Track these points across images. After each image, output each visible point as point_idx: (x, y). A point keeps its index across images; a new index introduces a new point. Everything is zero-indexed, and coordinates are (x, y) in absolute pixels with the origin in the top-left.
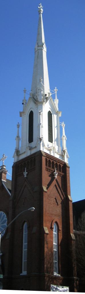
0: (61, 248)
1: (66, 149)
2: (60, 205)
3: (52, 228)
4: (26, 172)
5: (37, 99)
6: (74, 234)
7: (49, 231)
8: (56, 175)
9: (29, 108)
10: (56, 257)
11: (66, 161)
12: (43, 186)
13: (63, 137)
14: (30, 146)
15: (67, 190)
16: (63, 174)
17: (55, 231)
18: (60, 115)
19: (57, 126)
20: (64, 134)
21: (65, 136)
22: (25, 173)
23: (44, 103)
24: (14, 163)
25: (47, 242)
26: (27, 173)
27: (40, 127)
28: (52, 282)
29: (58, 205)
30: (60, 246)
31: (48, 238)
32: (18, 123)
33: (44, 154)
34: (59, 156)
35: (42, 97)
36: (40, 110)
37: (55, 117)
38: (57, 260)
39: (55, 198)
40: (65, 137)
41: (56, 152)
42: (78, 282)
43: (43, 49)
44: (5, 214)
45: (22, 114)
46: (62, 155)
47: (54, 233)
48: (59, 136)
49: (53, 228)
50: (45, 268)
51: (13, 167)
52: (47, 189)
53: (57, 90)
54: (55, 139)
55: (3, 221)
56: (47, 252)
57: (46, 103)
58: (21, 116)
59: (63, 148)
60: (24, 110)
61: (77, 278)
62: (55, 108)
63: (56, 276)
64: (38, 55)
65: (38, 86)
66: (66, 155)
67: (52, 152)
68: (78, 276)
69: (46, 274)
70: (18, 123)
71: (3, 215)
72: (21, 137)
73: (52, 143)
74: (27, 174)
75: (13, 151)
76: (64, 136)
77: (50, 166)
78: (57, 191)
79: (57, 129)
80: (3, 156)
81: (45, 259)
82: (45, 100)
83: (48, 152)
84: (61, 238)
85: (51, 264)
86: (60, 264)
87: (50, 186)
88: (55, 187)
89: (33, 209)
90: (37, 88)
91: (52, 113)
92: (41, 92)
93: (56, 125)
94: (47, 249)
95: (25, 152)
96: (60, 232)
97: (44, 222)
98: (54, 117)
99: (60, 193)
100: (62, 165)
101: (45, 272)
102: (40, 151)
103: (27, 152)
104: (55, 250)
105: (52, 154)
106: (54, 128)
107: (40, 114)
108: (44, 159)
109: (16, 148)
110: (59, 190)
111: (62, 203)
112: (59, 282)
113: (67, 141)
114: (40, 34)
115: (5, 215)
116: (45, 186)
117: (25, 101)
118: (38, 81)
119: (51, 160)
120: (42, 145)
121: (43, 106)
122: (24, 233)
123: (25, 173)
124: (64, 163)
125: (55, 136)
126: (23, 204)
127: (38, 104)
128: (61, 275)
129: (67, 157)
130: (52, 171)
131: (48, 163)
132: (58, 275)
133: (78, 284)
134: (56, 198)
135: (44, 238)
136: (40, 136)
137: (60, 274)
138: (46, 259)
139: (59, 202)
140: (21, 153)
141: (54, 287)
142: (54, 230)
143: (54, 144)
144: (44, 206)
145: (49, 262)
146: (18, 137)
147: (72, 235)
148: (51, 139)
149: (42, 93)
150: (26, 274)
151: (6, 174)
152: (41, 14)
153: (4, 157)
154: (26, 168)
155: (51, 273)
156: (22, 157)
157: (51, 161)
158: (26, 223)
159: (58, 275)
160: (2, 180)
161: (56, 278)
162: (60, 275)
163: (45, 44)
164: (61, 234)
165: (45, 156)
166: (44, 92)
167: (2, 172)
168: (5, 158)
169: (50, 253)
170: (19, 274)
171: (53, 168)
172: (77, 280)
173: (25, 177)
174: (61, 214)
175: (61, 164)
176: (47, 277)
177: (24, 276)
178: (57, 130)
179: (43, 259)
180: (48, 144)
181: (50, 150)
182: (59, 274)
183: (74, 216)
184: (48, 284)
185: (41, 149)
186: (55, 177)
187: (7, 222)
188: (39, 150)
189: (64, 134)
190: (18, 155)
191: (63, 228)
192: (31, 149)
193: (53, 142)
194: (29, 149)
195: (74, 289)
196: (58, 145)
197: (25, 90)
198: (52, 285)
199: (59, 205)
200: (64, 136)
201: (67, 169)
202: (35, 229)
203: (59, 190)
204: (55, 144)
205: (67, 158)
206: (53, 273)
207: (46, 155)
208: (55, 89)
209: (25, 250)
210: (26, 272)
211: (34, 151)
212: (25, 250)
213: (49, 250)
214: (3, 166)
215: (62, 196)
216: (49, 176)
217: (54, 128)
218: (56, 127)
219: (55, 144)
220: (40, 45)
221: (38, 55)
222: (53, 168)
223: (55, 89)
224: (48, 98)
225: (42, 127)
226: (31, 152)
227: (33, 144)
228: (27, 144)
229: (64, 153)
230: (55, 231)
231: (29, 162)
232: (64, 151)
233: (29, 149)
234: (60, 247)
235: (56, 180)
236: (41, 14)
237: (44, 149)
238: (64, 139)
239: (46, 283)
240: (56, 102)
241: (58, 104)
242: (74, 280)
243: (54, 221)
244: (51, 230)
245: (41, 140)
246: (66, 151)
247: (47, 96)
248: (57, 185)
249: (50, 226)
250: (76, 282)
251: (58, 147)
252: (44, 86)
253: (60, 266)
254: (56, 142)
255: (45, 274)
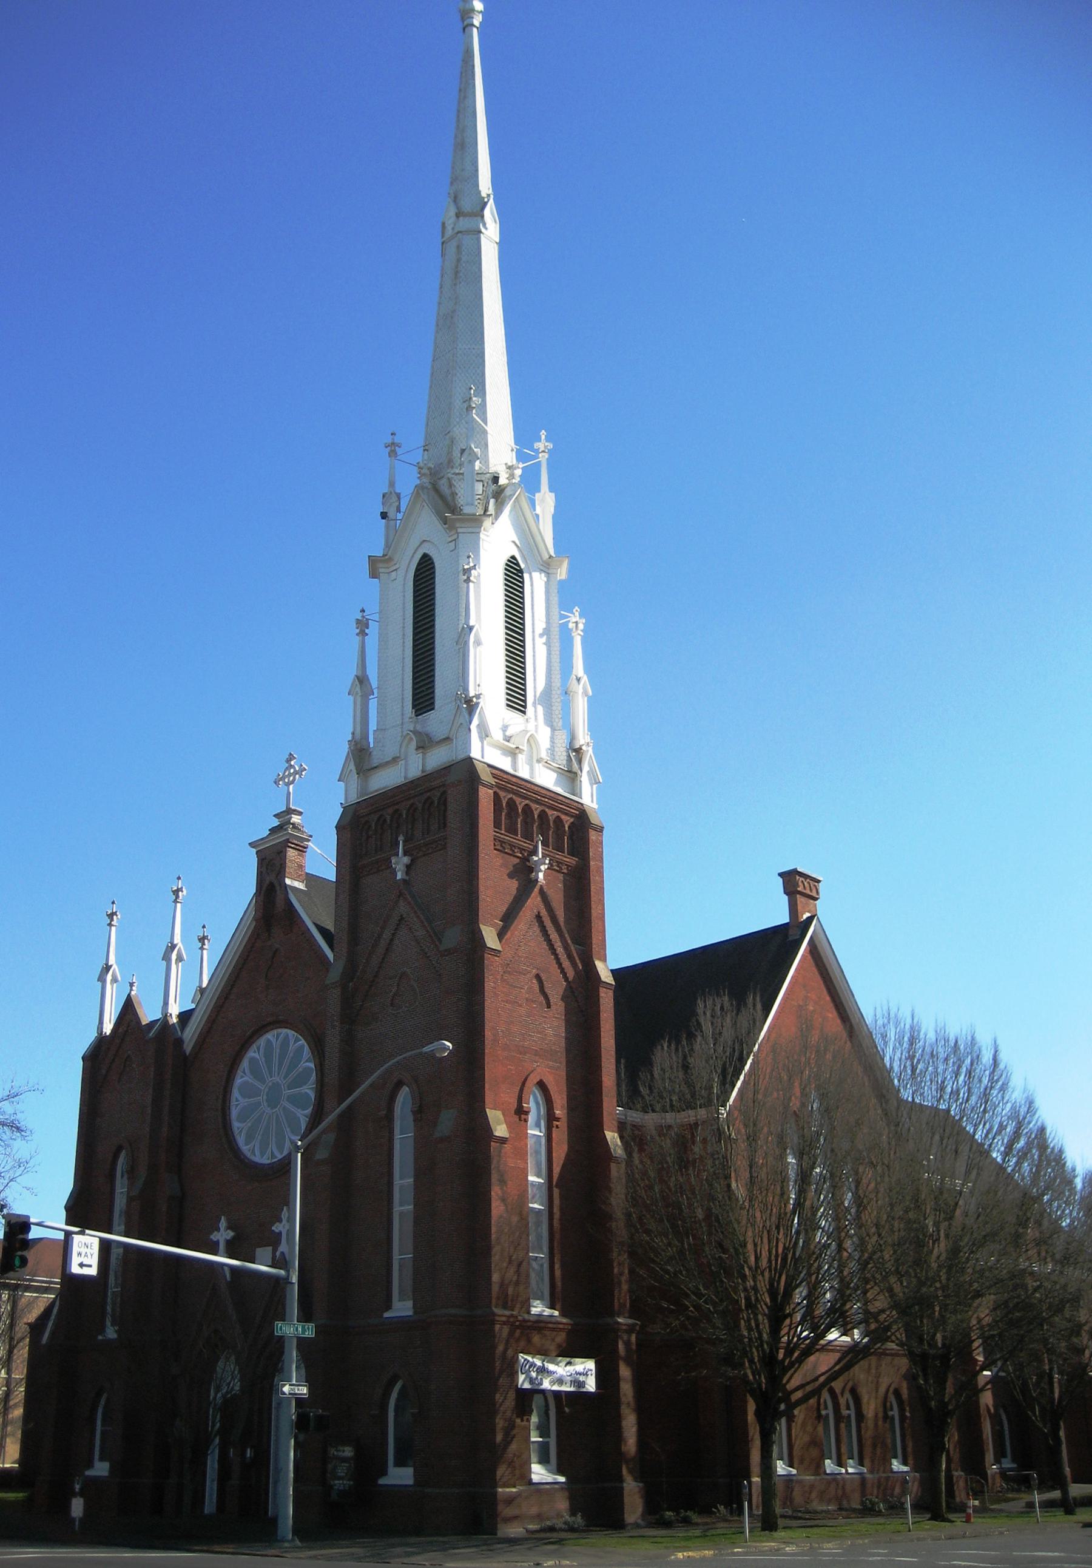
0: (562, 1197)
1: (588, 739)
2: (558, 1006)
3: (521, 1112)
4: (405, 854)
5: (454, 494)
6: (621, 1128)
7: (510, 1127)
8: (543, 868)
9: (414, 542)
10: (539, 1237)
11: (588, 797)
12: (482, 927)
13: (575, 682)
14: (419, 728)
15: (590, 937)
16: (572, 861)
17: (538, 1125)
18: (562, 573)
19: (547, 632)
20: (579, 667)
21: (585, 679)
22: (400, 863)
23: (487, 523)
24: (346, 809)
25: (502, 1176)
26: (406, 860)
27: (466, 643)
28: (522, 1343)
29: (549, 1006)
30: (557, 1186)
31: (504, 1160)
32: (363, 611)
33: (485, 776)
34: (555, 775)
35: (479, 488)
36: (469, 557)
37: (535, 586)
38: (546, 1249)
39: (538, 977)
40: (582, 682)
41: (539, 761)
42: (633, 1338)
43: (480, 232)
44: (303, 1042)
45: (381, 565)
46: (569, 771)
47: (529, 1132)
48: (557, 682)
49: (527, 1113)
50: (495, 1288)
51: (339, 828)
52: (501, 935)
53: (550, 446)
54: (538, 695)
55: (294, 1074)
56: (501, 1217)
57: (496, 518)
58: (374, 574)
59: (572, 737)
60: (388, 546)
61: (630, 1321)
62: (538, 538)
63: (540, 1315)
64: (459, 260)
65: (458, 431)
66: (586, 768)
67: (521, 758)
68: (635, 1311)
69: (496, 1310)
70: (363, 611)
71: (292, 1047)
72: (374, 683)
73: (524, 712)
74: (408, 867)
75: (343, 750)
76: (578, 680)
77: (512, 830)
78: (545, 945)
79: (548, 644)
80: (288, 761)
81: (494, 1251)
82: (492, 501)
83: (504, 763)
84: (561, 1152)
85: (520, 1265)
86: (557, 1266)
87: (512, 923)
88: (536, 929)
89: (446, 1048)
90: (452, 441)
91: (523, 566)
92: (471, 462)
93: (541, 626)
94: (502, 1208)
95: (395, 760)
96: (557, 1127)
97: (487, 1086)
98: (532, 585)
99: (560, 950)
100: (567, 820)
101: (494, 1301)
102: (470, 759)
103: (406, 759)
104: (536, 1206)
105: (524, 772)
106: (534, 640)
107: (468, 580)
108: (485, 796)
109: (353, 734)
110: (554, 936)
111: (570, 995)
112: (553, 1340)
113: (592, 702)
114: (465, 145)
115: (306, 1048)
116: (492, 926)
117: (394, 498)
118: (458, 403)
119: (518, 800)
120: (479, 733)
121: (482, 536)
122: (397, 1136)
123: (400, 863)
124: (577, 809)
125: (536, 680)
126: (392, 1004)
127: (458, 525)
128: (563, 1314)
129: (594, 781)
130: (522, 850)
131: (503, 814)
132: (547, 1312)
133: (634, 1347)
134: (542, 975)
135: (488, 1159)
136: (466, 689)
137: (558, 1306)
138: (496, 1250)
139: (556, 989)
140: (377, 758)
141: (533, 1365)
142: (532, 1118)
143: (532, 720)
144: (487, 1014)
145: (510, 1257)
146: (362, 680)
147: (612, 1137)
148: (517, 700)
149: (477, 468)
150: (411, 1313)
151: (302, 850)
152: (475, 30)
153: (292, 766)
154: (401, 839)
155: (518, 1306)
156: (386, 780)
157: (521, 803)
158: (405, 1090)
159: (547, 1312)
160: (288, 881)
161: (540, 1324)
162: (556, 1313)
163: (491, 201)
164: (561, 1135)
165: (490, 787)
166: (486, 461)
167: (288, 841)
168: (296, 773)
169: (515, 1219)
170: (382, 1316)
171: (528, 836)
172: (631, 1329)
173: (399, 876)
174: (563, 1044)
175: (566, 814)
176: (504, 1323)
177: (402, 1324)
178: (545, 647)
179: (487, 1251)
180: (506, 722)
181: (513, 753)
182: (552, 1307)
183: (623, 1061)
184: (510, 1353)
185: (475, 754)
186: (537, 881)
187: (313, 1077)
188: (462, 756)
189: (579, 667)
190: (365, 768)
191: (571, 1109)
192: (425, 743)
193: (530, 709)
194: (418, 748)
195: (618, 1366)
196: (549, 721)
197: (393, 444)
198: (522, 1357)
199: (553, 1007)
200: (578, 680)
201: (593, 835)
202: (448, 1121)
203: (554, 936)
204: (536, 719)
205: (592, 785)
206: (529, 1306)
207: (494, 776)
208: (540, 440)
209: (403, 1206)
210: (409, 1304)
211: (437, 758)
212: (403, 1206)
213: (510, 1207)
214: (289, 811)
215: (566, 964)
216: (511, 876)
217: (534, 640)
218: (541, 636)
219: (536, 719)
220: (467, 205)
221: (459, 260)
222: (528, 836)
223: (540, 440)
224: (508, 492)
225: (478, 643)
226: (423, 759)
227: (436, 721)
228: (406, 720)
229: (580, 762)
230: (538, 1125)
231: (416, 809)
232: (580, 749)
233: (414, 744)
234: (556, 1192)
235: (542, 892)
236: (475, 30)
237: (486, 748)
238: (581, 691)
239: (501, 1348)
240: (546, 503)
241: (555, 517)
242: (615, 1329)
243: (533, 1080)
244: (520, 1120)
245: (471, 706)
246: (589, 752)
247: (503, 481)
248: (544, 913)
249: (544, 1404)
250: (625, 1337)
251: (553, 730)
252: (489, 428)
253: (558, 1273)
254: (540, 708)
255: (494, 1314)
